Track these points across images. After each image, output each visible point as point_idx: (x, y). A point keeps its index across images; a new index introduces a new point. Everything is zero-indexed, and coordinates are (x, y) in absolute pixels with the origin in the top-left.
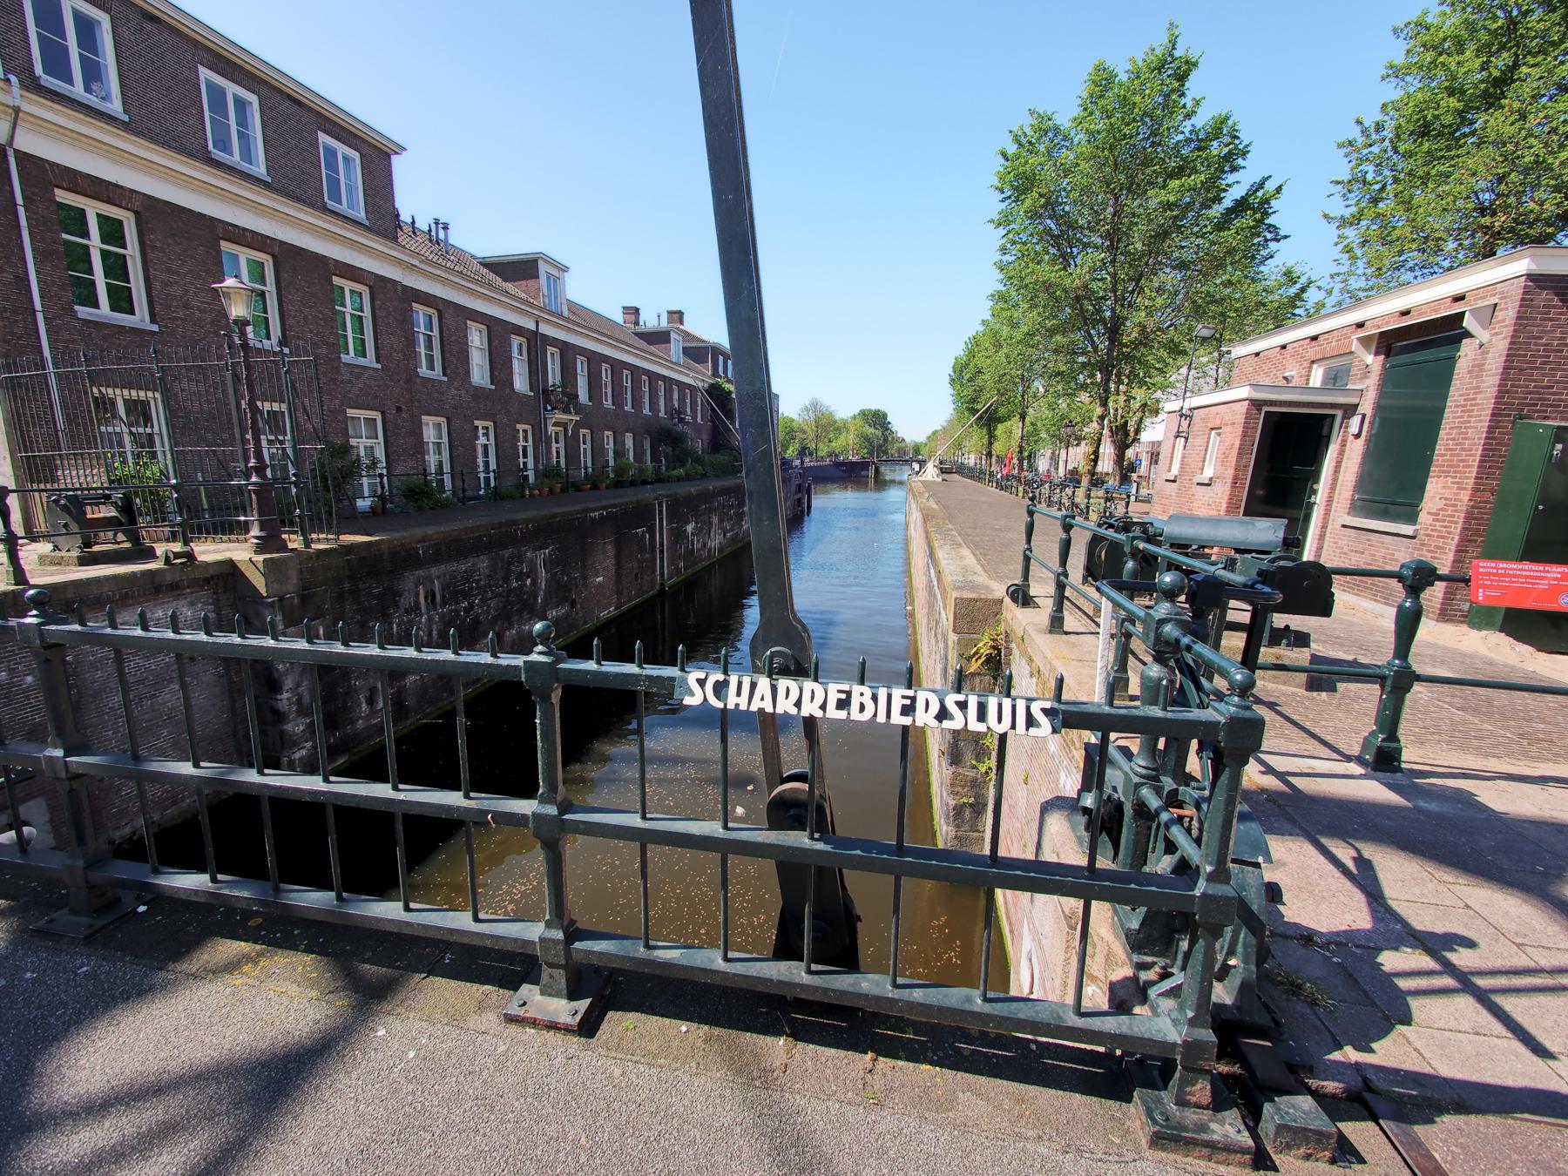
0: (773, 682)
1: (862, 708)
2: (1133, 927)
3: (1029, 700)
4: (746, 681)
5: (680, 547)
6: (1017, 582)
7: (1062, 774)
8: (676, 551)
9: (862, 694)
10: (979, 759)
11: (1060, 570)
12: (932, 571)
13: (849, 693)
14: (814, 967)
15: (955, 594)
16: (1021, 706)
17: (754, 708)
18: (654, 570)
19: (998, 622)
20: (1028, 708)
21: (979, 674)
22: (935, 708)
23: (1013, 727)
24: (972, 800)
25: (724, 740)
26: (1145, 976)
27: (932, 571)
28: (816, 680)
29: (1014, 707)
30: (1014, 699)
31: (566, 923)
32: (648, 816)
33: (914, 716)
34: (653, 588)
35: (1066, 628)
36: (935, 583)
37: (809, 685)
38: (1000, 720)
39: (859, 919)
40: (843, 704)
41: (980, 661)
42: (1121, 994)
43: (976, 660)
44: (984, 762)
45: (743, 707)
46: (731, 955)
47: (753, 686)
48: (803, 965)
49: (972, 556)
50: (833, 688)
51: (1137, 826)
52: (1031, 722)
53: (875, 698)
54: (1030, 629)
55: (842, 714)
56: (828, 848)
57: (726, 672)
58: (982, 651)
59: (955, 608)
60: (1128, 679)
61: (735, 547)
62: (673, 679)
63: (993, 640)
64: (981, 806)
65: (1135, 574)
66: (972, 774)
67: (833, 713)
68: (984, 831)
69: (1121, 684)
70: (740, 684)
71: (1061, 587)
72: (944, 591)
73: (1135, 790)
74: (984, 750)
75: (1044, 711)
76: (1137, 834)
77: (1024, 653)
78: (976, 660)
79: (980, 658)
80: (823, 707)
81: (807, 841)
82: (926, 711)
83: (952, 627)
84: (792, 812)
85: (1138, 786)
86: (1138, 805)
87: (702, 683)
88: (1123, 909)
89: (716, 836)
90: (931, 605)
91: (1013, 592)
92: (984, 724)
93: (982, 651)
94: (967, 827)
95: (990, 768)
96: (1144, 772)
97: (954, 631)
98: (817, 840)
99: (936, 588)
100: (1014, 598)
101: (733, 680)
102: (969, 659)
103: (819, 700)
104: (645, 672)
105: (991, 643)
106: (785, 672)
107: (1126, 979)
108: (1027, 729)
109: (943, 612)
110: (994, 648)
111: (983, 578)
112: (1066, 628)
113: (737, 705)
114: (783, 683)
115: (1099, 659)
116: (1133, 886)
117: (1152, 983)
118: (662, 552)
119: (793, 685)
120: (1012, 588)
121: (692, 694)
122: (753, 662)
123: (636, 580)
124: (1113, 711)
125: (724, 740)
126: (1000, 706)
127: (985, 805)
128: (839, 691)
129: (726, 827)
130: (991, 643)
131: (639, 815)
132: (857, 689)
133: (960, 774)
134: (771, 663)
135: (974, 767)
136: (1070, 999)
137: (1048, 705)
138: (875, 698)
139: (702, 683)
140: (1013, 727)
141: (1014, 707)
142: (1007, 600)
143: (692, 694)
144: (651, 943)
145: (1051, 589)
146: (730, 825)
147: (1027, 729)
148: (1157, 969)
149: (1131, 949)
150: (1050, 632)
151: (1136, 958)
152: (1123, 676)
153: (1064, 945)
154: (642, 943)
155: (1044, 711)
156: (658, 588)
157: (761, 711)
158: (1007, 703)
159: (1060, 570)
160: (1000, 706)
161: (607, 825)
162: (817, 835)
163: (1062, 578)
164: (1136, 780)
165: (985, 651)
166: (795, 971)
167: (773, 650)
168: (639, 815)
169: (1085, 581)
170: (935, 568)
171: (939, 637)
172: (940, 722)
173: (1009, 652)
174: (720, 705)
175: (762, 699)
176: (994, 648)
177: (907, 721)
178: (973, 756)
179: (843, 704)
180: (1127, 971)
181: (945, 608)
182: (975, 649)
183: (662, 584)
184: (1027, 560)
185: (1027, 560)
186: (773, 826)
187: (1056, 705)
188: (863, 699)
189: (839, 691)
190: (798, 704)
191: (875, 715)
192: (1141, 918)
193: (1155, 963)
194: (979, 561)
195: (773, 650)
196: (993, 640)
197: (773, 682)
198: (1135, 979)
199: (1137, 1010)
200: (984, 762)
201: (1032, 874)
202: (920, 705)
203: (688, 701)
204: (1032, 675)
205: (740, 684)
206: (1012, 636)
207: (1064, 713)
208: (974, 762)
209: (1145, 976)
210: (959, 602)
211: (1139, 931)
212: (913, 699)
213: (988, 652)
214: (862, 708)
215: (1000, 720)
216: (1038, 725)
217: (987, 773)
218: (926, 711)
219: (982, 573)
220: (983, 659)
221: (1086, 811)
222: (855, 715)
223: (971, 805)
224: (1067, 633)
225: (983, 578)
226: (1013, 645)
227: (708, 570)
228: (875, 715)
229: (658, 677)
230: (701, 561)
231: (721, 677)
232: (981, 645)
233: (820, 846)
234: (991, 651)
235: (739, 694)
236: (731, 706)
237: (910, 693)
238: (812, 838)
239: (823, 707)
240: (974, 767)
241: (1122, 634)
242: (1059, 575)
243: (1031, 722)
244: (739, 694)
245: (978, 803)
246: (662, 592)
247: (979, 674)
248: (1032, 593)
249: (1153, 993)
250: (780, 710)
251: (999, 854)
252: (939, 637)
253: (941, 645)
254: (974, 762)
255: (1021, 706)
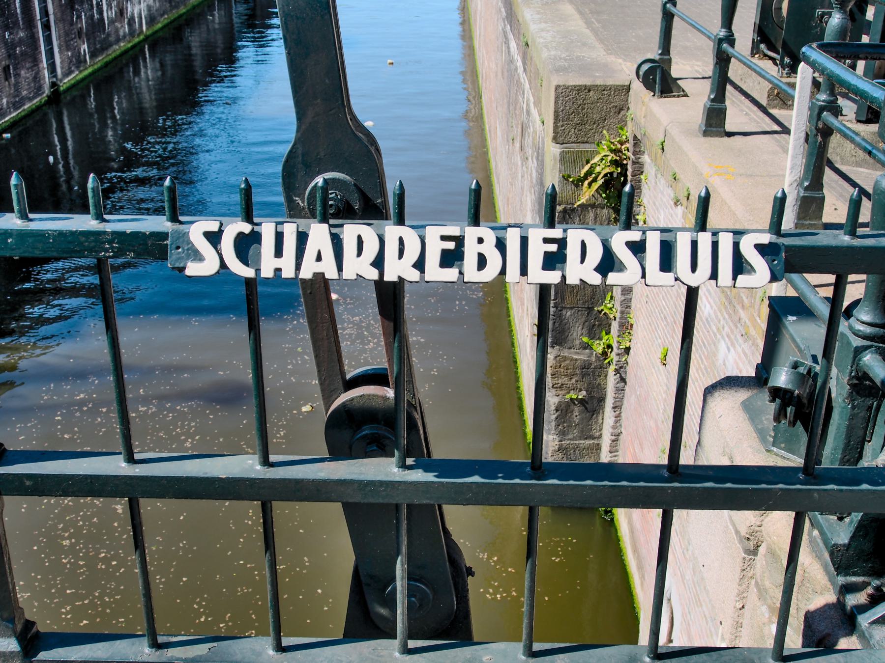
0: (334, 230)
1: (482, 262)
2: (840, 542)
3: (738, 233)
4: (290, 231)
5: (79, 17)
6: (650, 56)
7: (722, 346)
8: (72, 24)
9: (480, 241)
10: (593, 334)
11: (722, 33)
12: (513, 45)
13: (459, 241)
14: (412, 644)
15: (556, 80)
16: (726, 242)
17: (306, 273)
18: (36, 61)
19: (623, 124)
20: (736, 245)
21: (593, 206)
22: (595, 254)
23: (714, 276)
24: (582, 395)
25: (254, 328)
26: (854, 600)
27: (513, 45)
28: (401, 221)
29: (715, 245)
30: (715, 234)
31: (19, 627)
32: (137, 457)
33: (563, 270)
34: (39, 89)
35: (729, 127)
36: (519, 64)
37: (392, 232)
38: (694, 267)
39: (470, 572)
40: (451, 258)
41: (595, 186)
42: (822, 627)
43: (590, 185)
44: (600, 339)
45: (288, 273)
46: (286, 641)
47: (302, 238)
48: (396, 643)
49: (577, 16)
50: (433, 234)
51: (853, 407)
52: (740, 266)
53: (501, 245)
54: (674, 132)
55: (451, 274)
56: (430, 477)
57: (249, 218)
58: (598, 169)
59: (556, 102)
60: (823, 199)
61: (174, 14)
62: (163, 236)
63: (616, 151)
64: (595, 401)
65: (842, 32)
66: (582, 356)
67: (435, 272)
68: (600, 437)
69: (813, 207)
70: (279, 237)
71: (723, 60)
72: (535, 78)
73: (855, 357)
74: (600, 320)
75: (760, 248)
76: (852, 418)
77: (532, 182)
78: (590, 185)
79: (595, 180)
80: (420, 265)
81: (396, 470)
82: (582, 261)
83: (551, 133)
84: (366, 431)
85: (858, 352)
86: (857, 378)
87: (214, 238)
88: (827, 521)
89: (253, 476)
90: (512, 104)
91: (647, 73)
92: (670, 276)
93: (598, 169)
94: (575, 432)
95: (609, 346)
96: (868, 330)
97: (555, 139)
98: (410, 468)
99: (521, 70)
100: (648, 83)
101: (268, 231)
102: (578, 183)
103: (412, 252)
104: (109, 228)
105: (612, 156)
106: (346, 212)
107: (828, 607)
108: (735, 278)
109: (534, 112)
110: (616, 163)
111: (597, 53)
112: (729, 127)
113: (278, 270)
114: (351, 231)
115: (788, 171)
116: (865, 486)
117: (862, 609)
118: (47, 27)
119: (368, 233)
120: (645, 67)
121: (197, 256)
122: (290, 200)
123: (7, 78)
124: (857, 242)
125: (254, 328)
126: (694, 244)
127: (602, 400)
128: (444, 238)
129: (266, 462)
130: (612, 156)
131: (121, 457)
132: (471, 234)
133: (565, 358)
134: (325, 199)
135: (586, 346)
136: (770, 643)
137: (765, 238)
138: (501, 245)
139: (214, 238)
140: (714, 276)
141: (715, 245)
142: (638, 86)
143: (197, 256)
144: (161, 639)
145: (708, 66)
146: (273, 458)
147: (735, 278)
148: (870, 590)
149: (836, 569)
150: (706, 133)
151: (841, 580)
152: (816, 195)
153: (738, 575)
154: (145, 641)
155: (760, 248)
156: (47, 91)
157: (320, 277)
158: (705, 240)
159: (722, 33)
160: (694, 244)
161: (72, 477)
162: (410, 461)
163: (725, 45)
164: (857, 342)
165: (603, 169)
166: (385, 653)
167: (329, 175)
168: (121, 457)
169: (755, 50)
170: (517, 38)
171: (529, 151)
172: (604, 276)
173: (639, 169)
174: (249, 273)
175: (319, 258)
176: (616, 163)
177: (553, 277)
178: (585, 331)
179: (451, 258)
180: (831, 597)
181: (537, 103)
182: (587, 168)
183: (53, 85)
184: (668, 18)
185: (668, 18)
186: (337, 453)
187: (774, 238)
188: (482, 248)
189: (444, 238)
190: (379, 263)
191: (503, 272)
192: (852, 529)
193: (868, 584)
194: (588, 24)
195: (329, 175)
196: (616, 151)
197: (334, 230)
198: (840, 605)
199: (843, 643)
200: (600, 339)
201: (729, 485)
202: (573, 252)
203: (193, 269)
204: (677, 203)
205: (279, 237)
206: (645, 146)
207: (788, 248)
208: (585, 339)
209: (854, 600)
210: (562, 92)
211: (848, 546)
212: (562, 243)
213: (607, 170)
214: (482, 262)
215: (694, 267)
216: (752, 270)
217: (604, 354)
218: (582, 261)
219: (597, 45)
220: (600, 182)
221: (777, 393)
222: (471, 273)
223: (582, 402)
224: (730, 134)
225: (597, 53)
226: (646, 159)
227: (133, 57)
228: (503, 272)
229: (136, 235)
230: (118, 40)
231: (246, 228)
232: (596, 159)
233: (418, 476)
234: (612, 169)
235: (279, 253)
236: (267, 272)
237: (556, 233)
238: (403, 466)
239: (420, 265)
240: (586, 346)
241: (818, 130)
242: (720, 41)
243: (740, 266)
244: (279, 253)
245: (592, 398)
246: (56, 97)
247: (593, 206)
248: (675, 73)
249: (864, 620)
250: (349, 273)
251: (680, 463)
252: (529, 151)
253: (533, 164)
254: (585, 339)
255: (726, 242)
